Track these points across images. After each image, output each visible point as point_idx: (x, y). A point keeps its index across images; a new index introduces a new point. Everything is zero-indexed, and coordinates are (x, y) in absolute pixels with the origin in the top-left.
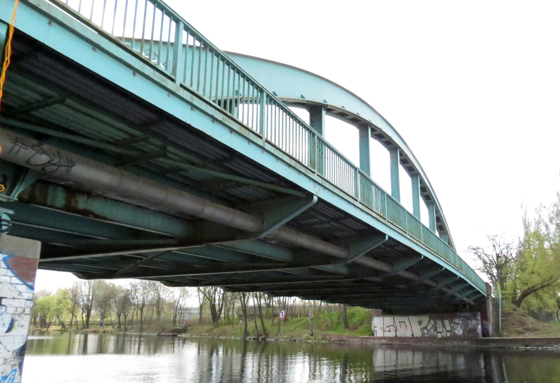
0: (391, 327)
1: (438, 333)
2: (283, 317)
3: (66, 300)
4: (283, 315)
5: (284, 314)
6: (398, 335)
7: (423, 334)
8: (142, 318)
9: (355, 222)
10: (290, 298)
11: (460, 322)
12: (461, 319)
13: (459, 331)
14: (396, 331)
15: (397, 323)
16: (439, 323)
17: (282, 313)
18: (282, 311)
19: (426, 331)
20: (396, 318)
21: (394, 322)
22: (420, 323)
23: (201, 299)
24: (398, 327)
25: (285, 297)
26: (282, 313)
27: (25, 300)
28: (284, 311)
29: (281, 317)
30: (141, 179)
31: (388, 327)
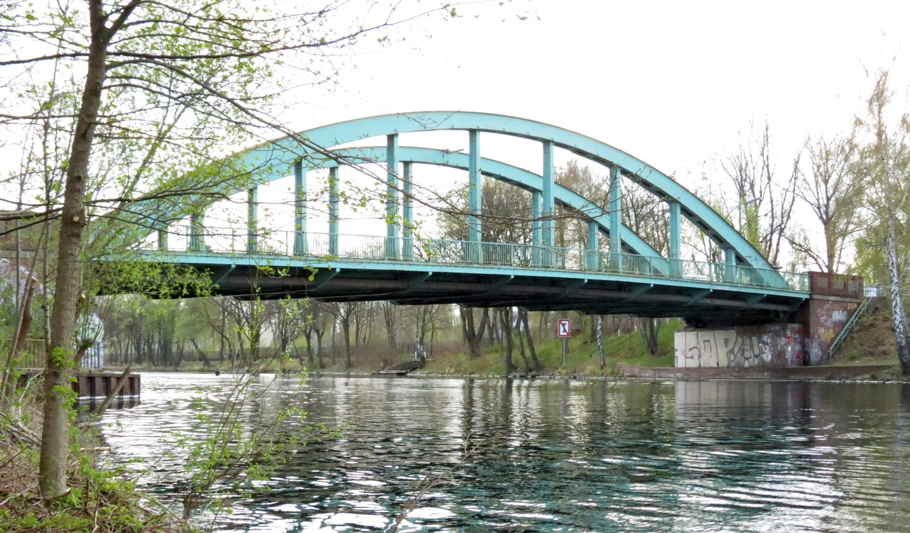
0: (695, 350)
1: (747, 359)
2: (565, 334)
3: (855, 224)
4: (565, 331)
5: (567, 327)
6: (702, 365)
7: (730, 361)
8: (460, 438)
9: (802, 509)
10: (638, 174)
11: (769, 341)
12: (770, 335)
13: (768, 357)
14: (700, 357)
15: (701, 343)
16: (747, 341)
17: (564, 325)
18: (563, 322)
19: (732, 357)
20: (700, 334)
21: (698, 342)
22: (726, 342)
23: (113, 84)
24: (702, 351)
25: (88, 52)
26: (564, 325)
27: (441, 153)
28: (567, 322)
29: (562, 333)
30: (66, 288)
31: (690, 349)
